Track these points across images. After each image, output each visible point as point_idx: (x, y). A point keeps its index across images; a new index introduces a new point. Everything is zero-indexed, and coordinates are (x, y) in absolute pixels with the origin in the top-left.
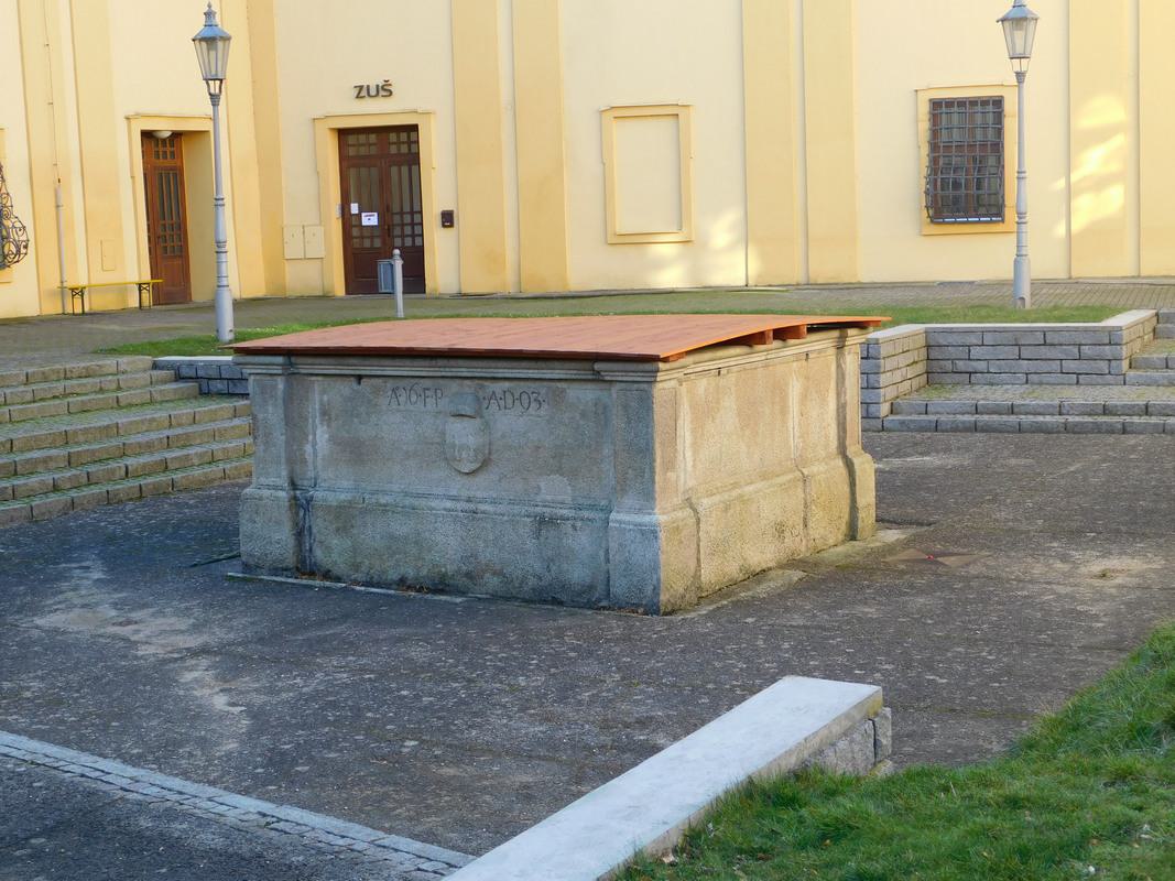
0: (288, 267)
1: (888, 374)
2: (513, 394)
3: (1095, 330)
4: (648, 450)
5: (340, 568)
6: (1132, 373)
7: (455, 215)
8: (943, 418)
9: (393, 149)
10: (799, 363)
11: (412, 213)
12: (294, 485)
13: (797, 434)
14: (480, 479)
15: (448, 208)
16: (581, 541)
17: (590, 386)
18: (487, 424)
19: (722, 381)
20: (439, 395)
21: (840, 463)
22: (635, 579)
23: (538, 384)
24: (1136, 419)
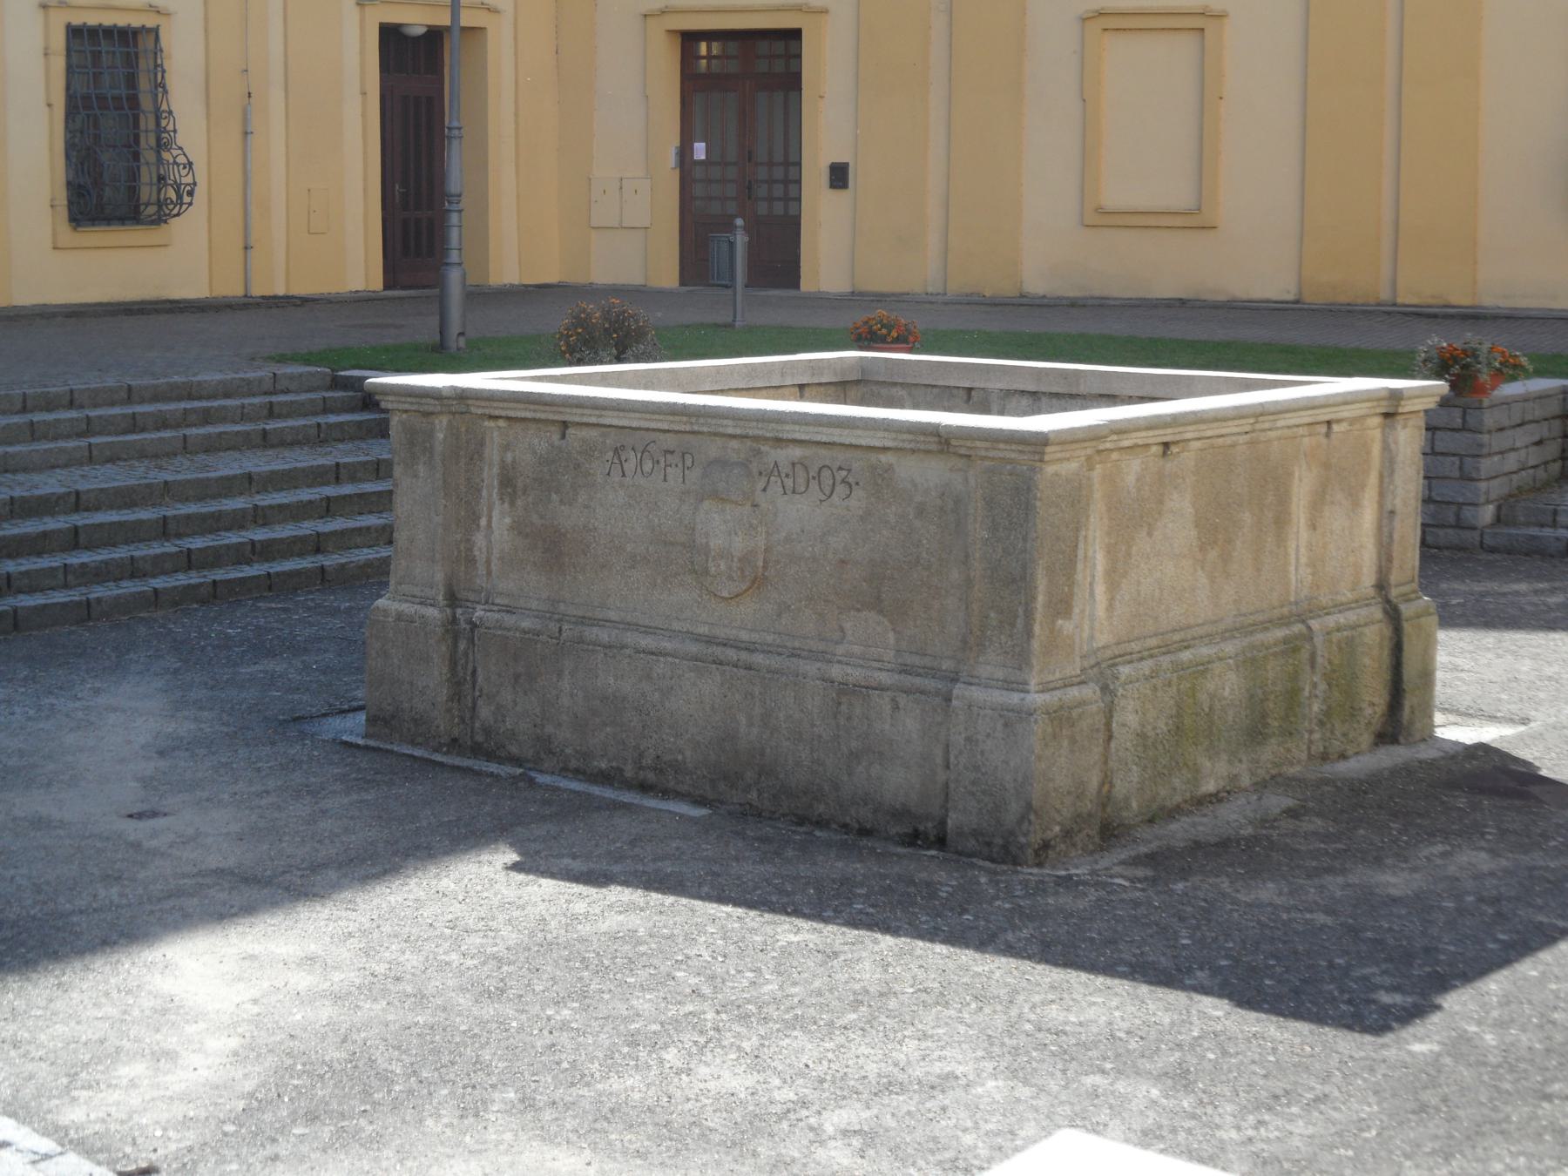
1: (1496, 458)
2: (806, 469)
4: (1023, 578)
7: (63, 213)
11: (787, 164)
12: (453, 599)
13: (1303, 560)
19: (1170, 466)
20: (689, 463)
22: (549, 936)
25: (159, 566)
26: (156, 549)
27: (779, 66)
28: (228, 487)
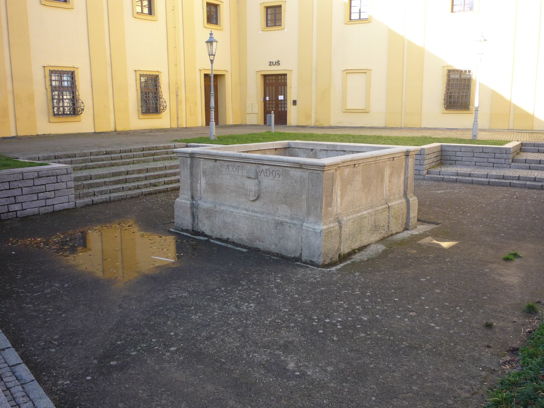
0: (248, 116)
3: (501, 148)
5: (208, 232)
6: (513, 164)
8: (445, 177)
9: (274, 81)
10: (390, 162)
12: (193, 198)
13: (387, 190)
14: (257, 203)
15: (295, 99)
16: (292, 233)
17: (298, 170)
18: (260, 182)
19: (356, 169)
21: (404, 200)
23: (279, 168)
24: (515, 182)
25: (146, 186)
26: (144, 183)
27: (283, 81)
28: (161, 169)
